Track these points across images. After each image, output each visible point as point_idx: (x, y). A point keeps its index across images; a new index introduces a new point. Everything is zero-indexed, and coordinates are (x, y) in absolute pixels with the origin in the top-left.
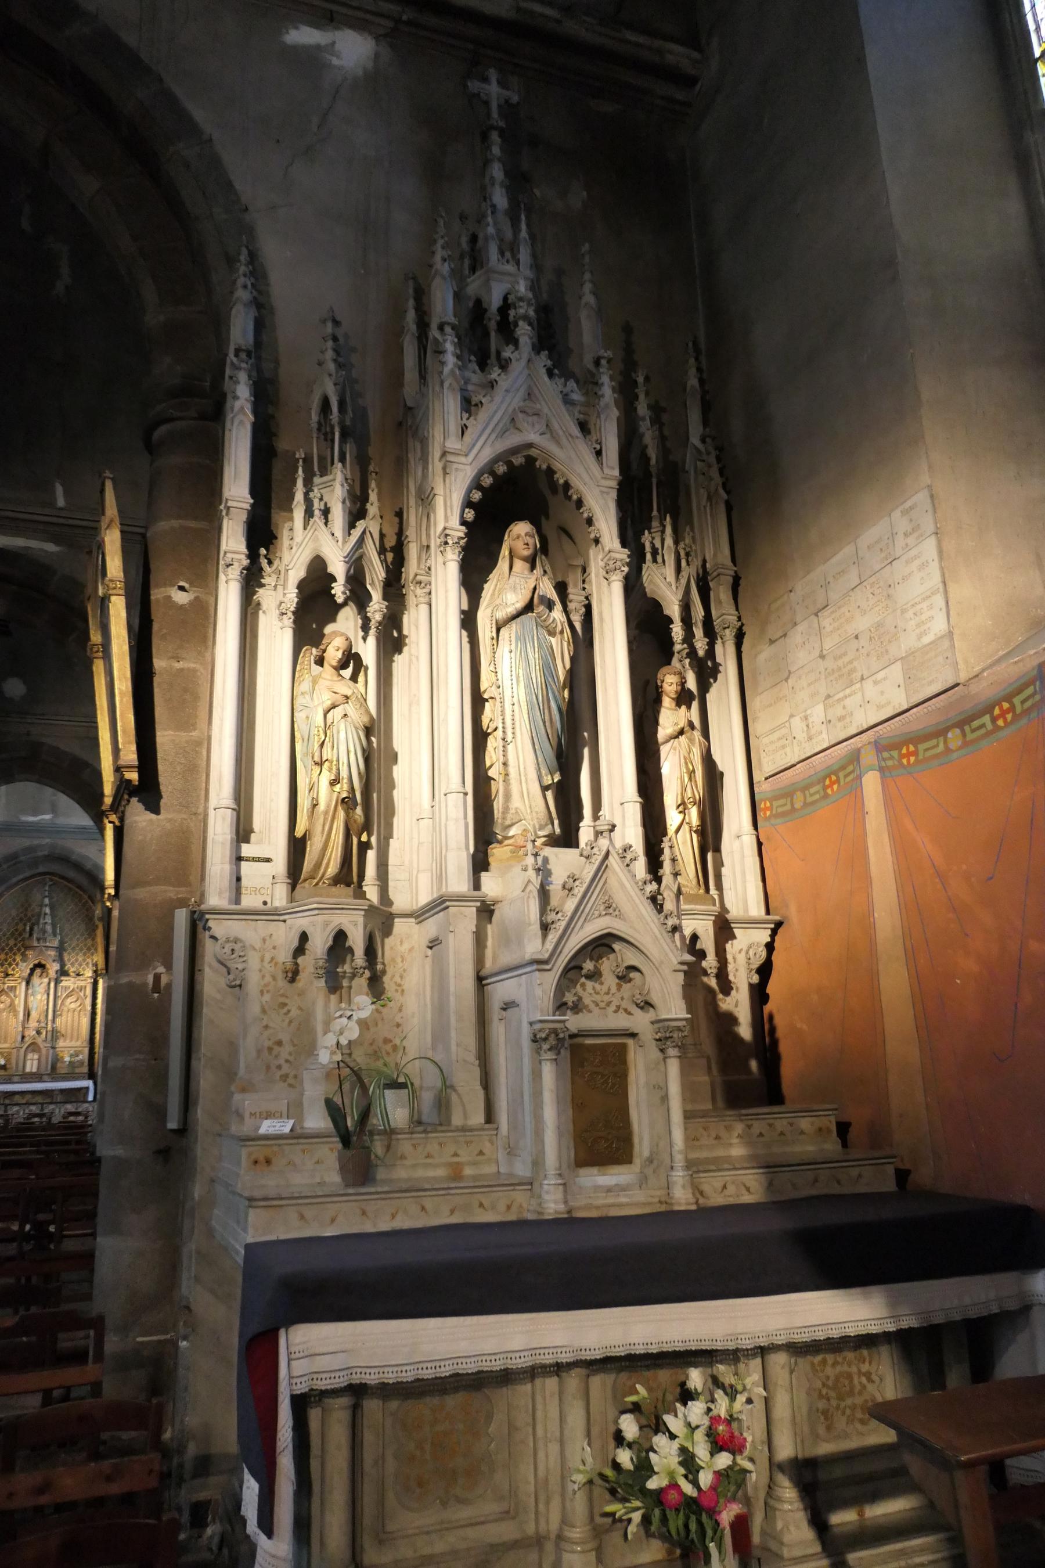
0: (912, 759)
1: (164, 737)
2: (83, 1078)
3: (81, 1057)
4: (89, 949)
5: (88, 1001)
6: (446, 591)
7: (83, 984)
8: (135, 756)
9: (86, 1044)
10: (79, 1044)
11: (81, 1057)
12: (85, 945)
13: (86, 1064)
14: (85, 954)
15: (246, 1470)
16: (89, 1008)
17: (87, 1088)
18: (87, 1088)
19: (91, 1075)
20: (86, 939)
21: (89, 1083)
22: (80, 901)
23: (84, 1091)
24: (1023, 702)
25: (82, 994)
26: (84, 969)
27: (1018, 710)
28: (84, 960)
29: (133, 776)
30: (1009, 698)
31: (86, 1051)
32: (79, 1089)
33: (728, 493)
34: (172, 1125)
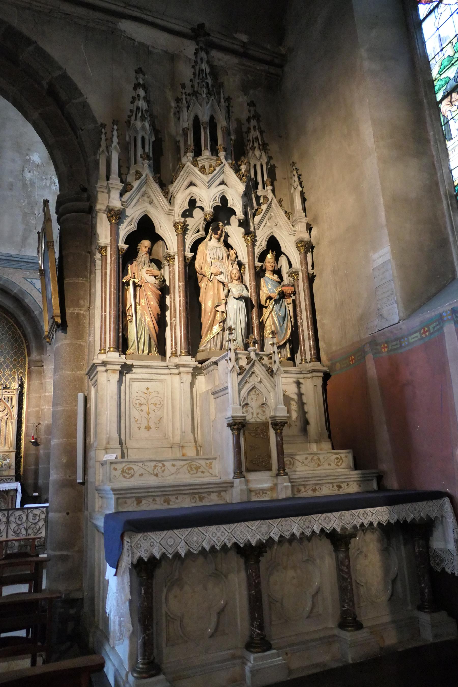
0: (386, 349)
1: (69, 311)
2: (11, 481)
3: (8, 461)
4: (15, 366)
5: (15, 411)
6: (268, 55)
7: (10, 395)
8: (59, 312)
9: (13, 449)
10: (6, 448)
11: (8, 461)
12: (11, 362)
13: (13, 467)
14: (11, 370)
15: (108, 565)
16: (15, 416)
17: (16, 490)
18: (16, 490)
19: (18, 478)
20: (12, 357)
21: (18, 486)
22: (7, 324)
23: (12, 493)
24: (434, 328)
25: (9, 404)
26: (10, 383)
27: (432, 331)
28: (11, 375)
29: (59, 320)
30: (428, 326)
31: (13, 455)
32: (7, 492)
33: (302, 188)
34: (80, 480)
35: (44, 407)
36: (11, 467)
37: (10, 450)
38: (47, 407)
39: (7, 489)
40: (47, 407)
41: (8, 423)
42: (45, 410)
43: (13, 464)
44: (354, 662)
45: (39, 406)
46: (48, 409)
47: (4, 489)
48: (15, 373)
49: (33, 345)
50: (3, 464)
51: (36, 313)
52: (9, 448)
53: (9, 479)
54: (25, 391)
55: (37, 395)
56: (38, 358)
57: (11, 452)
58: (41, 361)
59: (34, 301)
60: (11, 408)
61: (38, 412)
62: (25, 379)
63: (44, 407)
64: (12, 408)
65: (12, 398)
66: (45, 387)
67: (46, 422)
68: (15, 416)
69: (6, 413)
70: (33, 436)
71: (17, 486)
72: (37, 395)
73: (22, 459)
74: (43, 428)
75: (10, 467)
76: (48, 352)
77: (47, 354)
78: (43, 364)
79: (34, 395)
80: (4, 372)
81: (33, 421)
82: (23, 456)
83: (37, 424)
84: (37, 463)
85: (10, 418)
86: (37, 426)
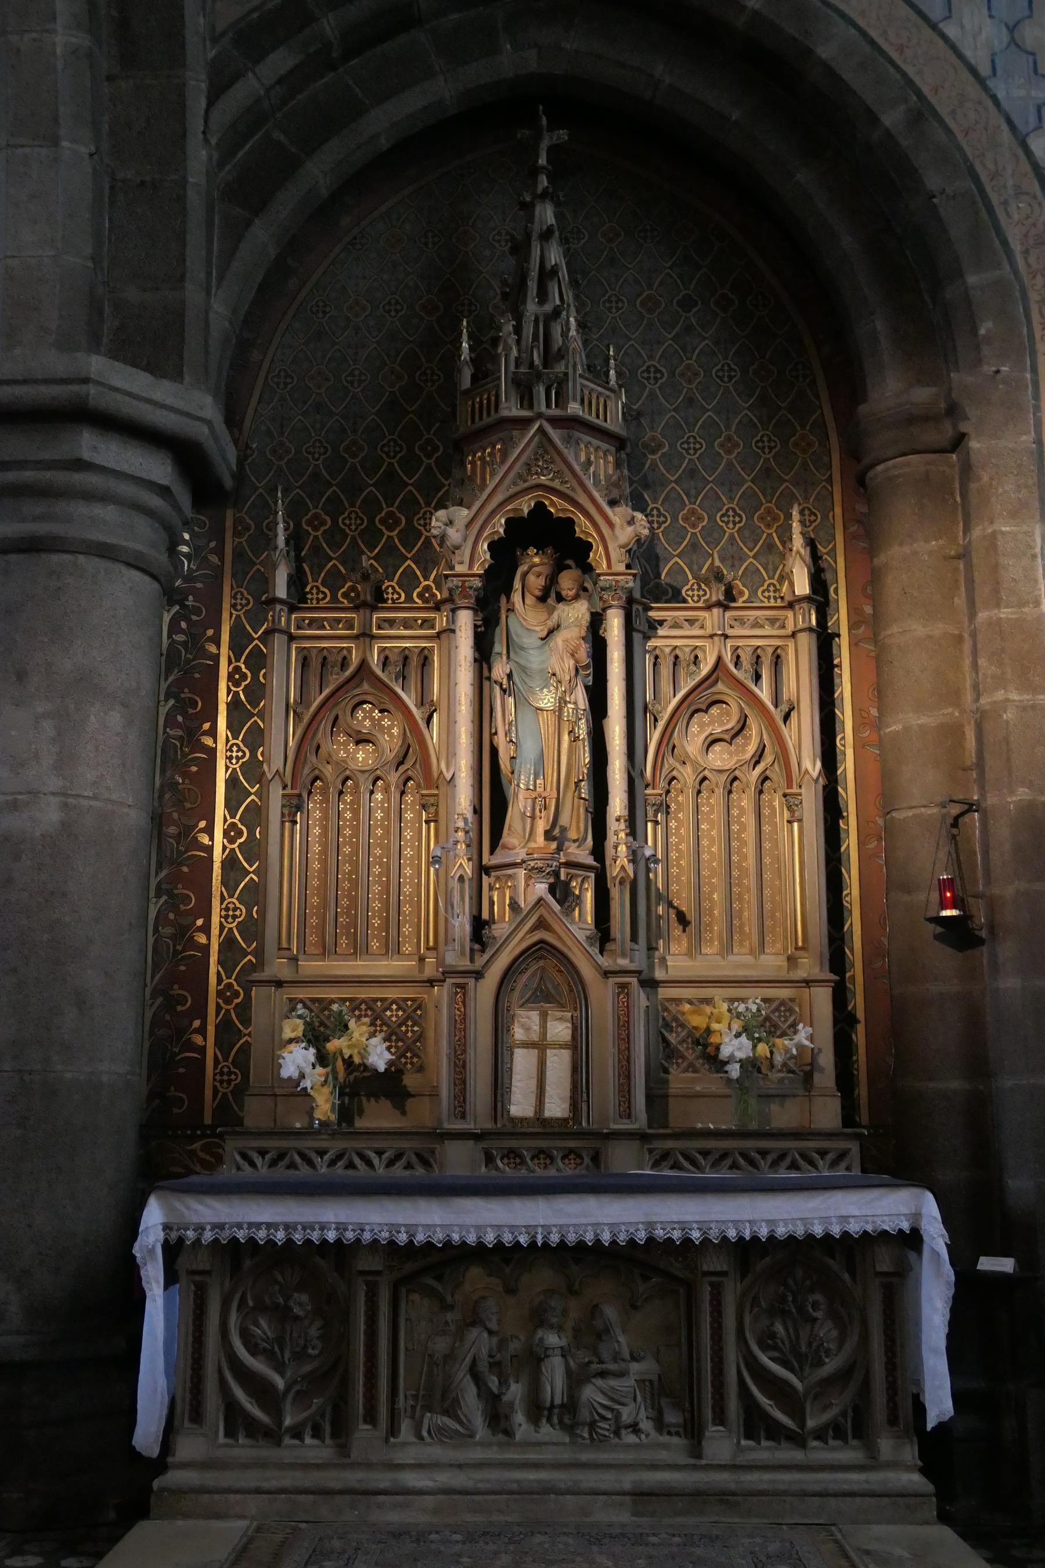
3: (802, 1035)
10: (772, 963)
17: (912, 1239)
25: (764, 694)
32: (851, 1248)
35: (1000, 695)
36: (817, 1076)
37: (801, 974)
38: (1014, 696)
39: (854, 1228)
40: (1014, 696)
41: (766, 812)
42: (1008, 716)
43: (827, 1060)
44: (331, 1055)
45: (954, 696)
46: (1023, 708)
47: (836, 1230)
48: (775, 519)
49: (875, 327)
50: (779, 1059)
51: (891, 118)
52: (791, 960)
53: (823, 1153)
54: (841, 619)
55: (939, 628)
56: (923, 395)
57: (808, 983)
58: (953, 411)
59: (867, 49)
60: (777, 715)
61: (952, 732)
62: (833, 553)
63: (1000, 695)
64: (787, 717)
65: (777, 661)
66: (995, 568)
67: (1022, 794)
68: (807, 764)
69: (752, 749)
70: (944, 885)
71: (917, 1216)
72: (939, 628)
73: (861, 1028)
74: (1002, 832)
75: (808, 1078)
76: (986, 350)
77: (979, 362)
78: (963, 427)
79: (919, 629)
80: (712, 518)
81: (923, 795)
82: (860, 1015)
83: (955, 810)
84: (978, 1064)
85: (776, 774)
86: (955, 824)
